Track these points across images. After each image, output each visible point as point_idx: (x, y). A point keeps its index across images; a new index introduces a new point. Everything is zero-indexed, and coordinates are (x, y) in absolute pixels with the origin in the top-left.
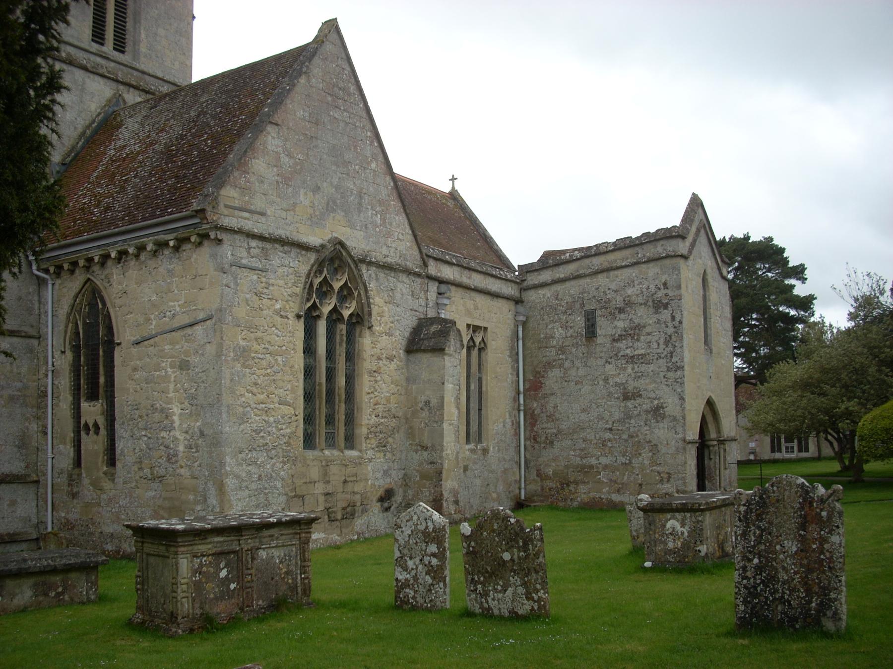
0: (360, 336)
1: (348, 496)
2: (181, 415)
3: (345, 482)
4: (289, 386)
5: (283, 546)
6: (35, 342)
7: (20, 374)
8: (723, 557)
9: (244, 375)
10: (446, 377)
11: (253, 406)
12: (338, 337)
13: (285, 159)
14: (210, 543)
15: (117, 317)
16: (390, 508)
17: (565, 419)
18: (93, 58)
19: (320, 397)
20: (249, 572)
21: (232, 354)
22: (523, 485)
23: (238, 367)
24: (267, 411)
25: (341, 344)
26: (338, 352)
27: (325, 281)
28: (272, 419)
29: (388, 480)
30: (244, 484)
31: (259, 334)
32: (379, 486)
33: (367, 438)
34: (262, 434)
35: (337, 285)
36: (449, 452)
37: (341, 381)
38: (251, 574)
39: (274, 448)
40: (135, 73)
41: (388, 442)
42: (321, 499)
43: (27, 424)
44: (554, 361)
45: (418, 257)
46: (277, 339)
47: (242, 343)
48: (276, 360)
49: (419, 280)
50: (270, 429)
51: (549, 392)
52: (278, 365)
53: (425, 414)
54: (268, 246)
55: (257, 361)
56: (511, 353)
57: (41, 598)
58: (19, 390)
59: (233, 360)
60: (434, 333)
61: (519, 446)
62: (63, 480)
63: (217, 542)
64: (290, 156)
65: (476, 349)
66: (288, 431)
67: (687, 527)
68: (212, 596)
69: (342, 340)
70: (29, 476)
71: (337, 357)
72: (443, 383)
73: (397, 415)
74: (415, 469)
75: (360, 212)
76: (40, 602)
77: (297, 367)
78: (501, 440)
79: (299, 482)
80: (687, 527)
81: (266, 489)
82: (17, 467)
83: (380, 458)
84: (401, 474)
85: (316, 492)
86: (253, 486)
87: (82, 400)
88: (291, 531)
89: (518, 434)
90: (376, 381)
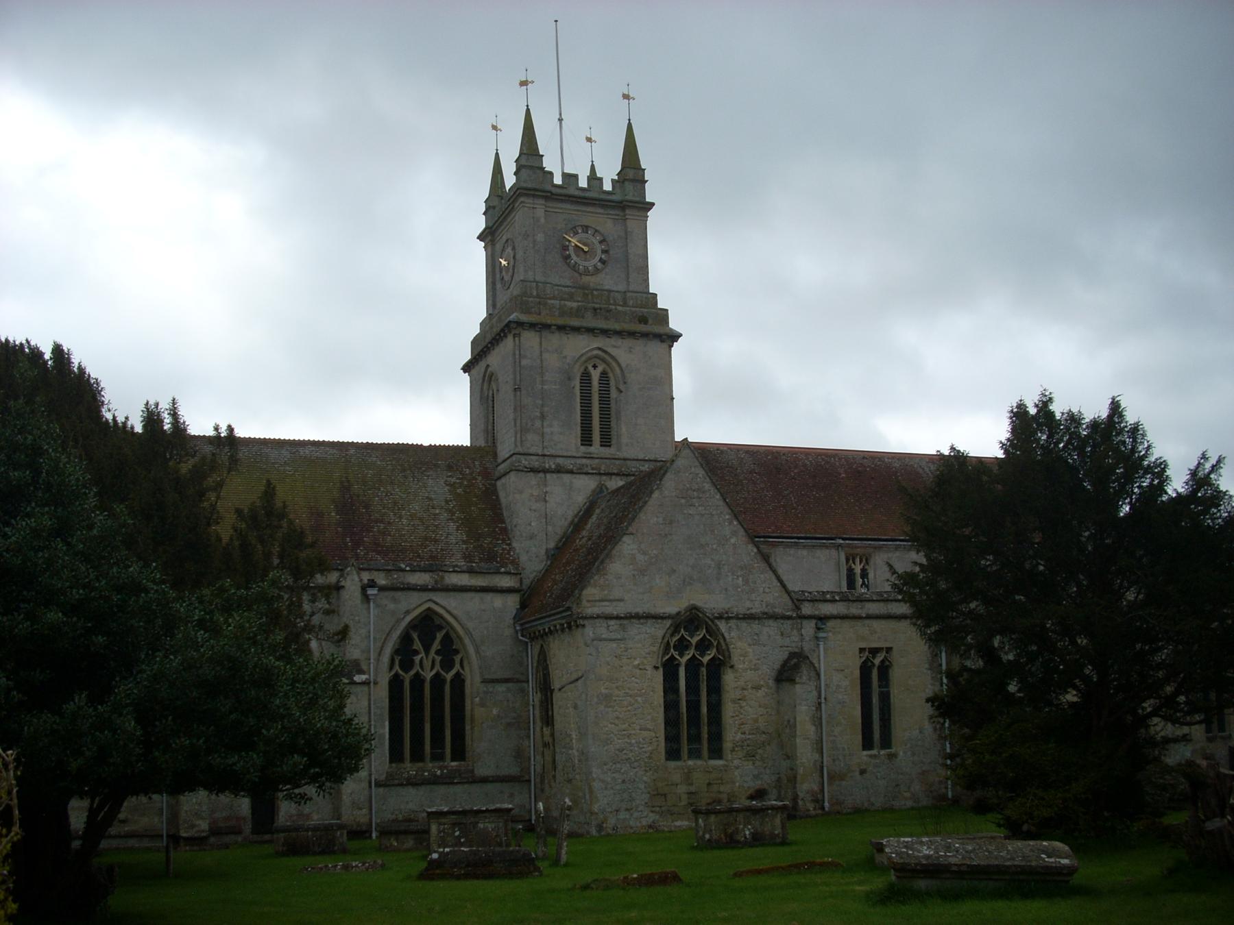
3: (709, 784)
13: (640, 557)
18: (579, 461)
23: (602, 707)
24: (629, 736)
27: (682, 638)
31: (620, 683)
35: (694, 641)
37: (704, 710)
40: (617, 462)
45: (790, 603)
47: (603, 691)
49: (789, 622)
53: (787, 731)
54: (625, 622)
64: (644, 553)
75: (718, 579)
82: (514, 770)
83: (748, 766)
84: (774, 778)
86: (618, 787)
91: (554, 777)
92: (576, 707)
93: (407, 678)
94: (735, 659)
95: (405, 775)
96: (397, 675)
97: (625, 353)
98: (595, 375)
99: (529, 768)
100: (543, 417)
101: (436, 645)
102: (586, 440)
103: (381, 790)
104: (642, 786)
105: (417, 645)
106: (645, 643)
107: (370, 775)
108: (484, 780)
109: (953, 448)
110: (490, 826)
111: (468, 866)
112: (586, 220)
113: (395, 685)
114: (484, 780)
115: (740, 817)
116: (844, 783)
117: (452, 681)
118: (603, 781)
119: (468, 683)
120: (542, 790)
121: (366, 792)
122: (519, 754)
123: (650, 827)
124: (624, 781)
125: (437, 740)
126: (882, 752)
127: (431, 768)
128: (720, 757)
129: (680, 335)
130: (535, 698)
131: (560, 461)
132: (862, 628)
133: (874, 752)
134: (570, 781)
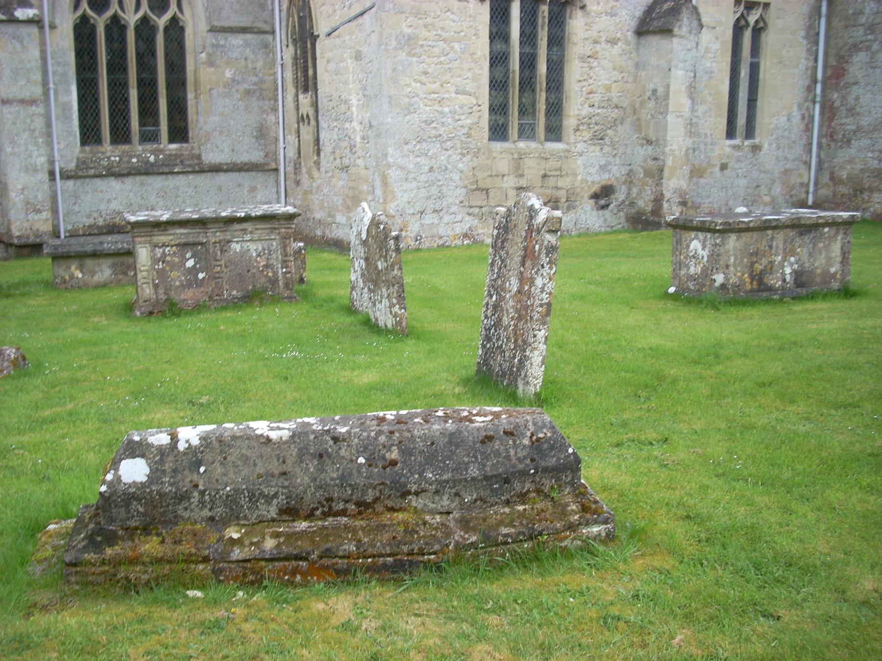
0: (570, 18)
1: (549, 191)
2: (357, 105)
3: (545, 176)
4: (469, 74)
5: (260, 240)
6: (269, 38)
7: (255, 68)
8: (759, 291)
9: (410, 64)
10: (674, 63)
11: (422, 95)
12: (540, 20)
14: (173, 234)
15: (315, 10)
16: (608, 206)
17: (867, 114)
19: (514, 86)
20: (218, 263)
21: (394, 43)
22: (811, 189)
23: (403, 56)
25: (543, 28)
26: (540, 37)
28: (446, 110)
29: (607, 176)
30: (411, 176)
31: (429, 20)
32: (593, 182)
33: (577, 130)
34: (434, 125)
36: (675, 147)
37: (542, 68)
38: (220, 266)
39: (450, 139)
41: (606, 135)
42: (512, 193)
43: (265, 116)
44: (861, 42)
46: (453, 24)
47: (407, 31)
48: (453, 47)
50: (444, 120)
51: (852, 80)
52: (455, 52)
53: (651, 104)
55: (427, 49)
56: (808, 33)
57: (120, 277)
58: (255, 84)
59: (396, 49)
60: (665, 12)
61: (811, 144)
62: (290, 169)
63: (181, 234)
65: (750, 29)
66: (469, 121)
67: (707, 250)
68: (178, 283)
69: (544, 23)
70: (268, 164)
71: (539, 42)
72: (670, 70)
73: (620, 105)
74: (639, 165)
76: (120, 280)
77: (479, 53)
78: (783, 137)
79: (481, 175)
80: (707, 250)
81: (439, 181)
82: (256, 156)
84: (624, 170)
85: (505, 185)
86: (423, 178)
87: (300, 92)
88: (268, 226)
89: (808, 129)
90: (591, 68)
91: (317, 164)
92: (358, 57)
93: (101, 22)
95: (105, 163)
96: (84, 18)
99: (275, 153)
103: (70, 183)
104: (456, 177)
107: (52, 162)
108: (216, 169)
110: (254, 248)
111: (290, 512)
113: (83, 33)
114: (216, 169)
115: (780, 238)
116: (702, 181)
117: (167, 29)
118: (402, 168)
119: (189, 32)
120: (298, 183)
121: (46, 187)
122: (262, 134)
123: (466, 236)
124: (431, 169)
125: (148, 112)
126: (747, 143)
127: (140, 152)
128: (559, 139)
130: (285, 53)
133: (737, 141)
134: (345, 168)
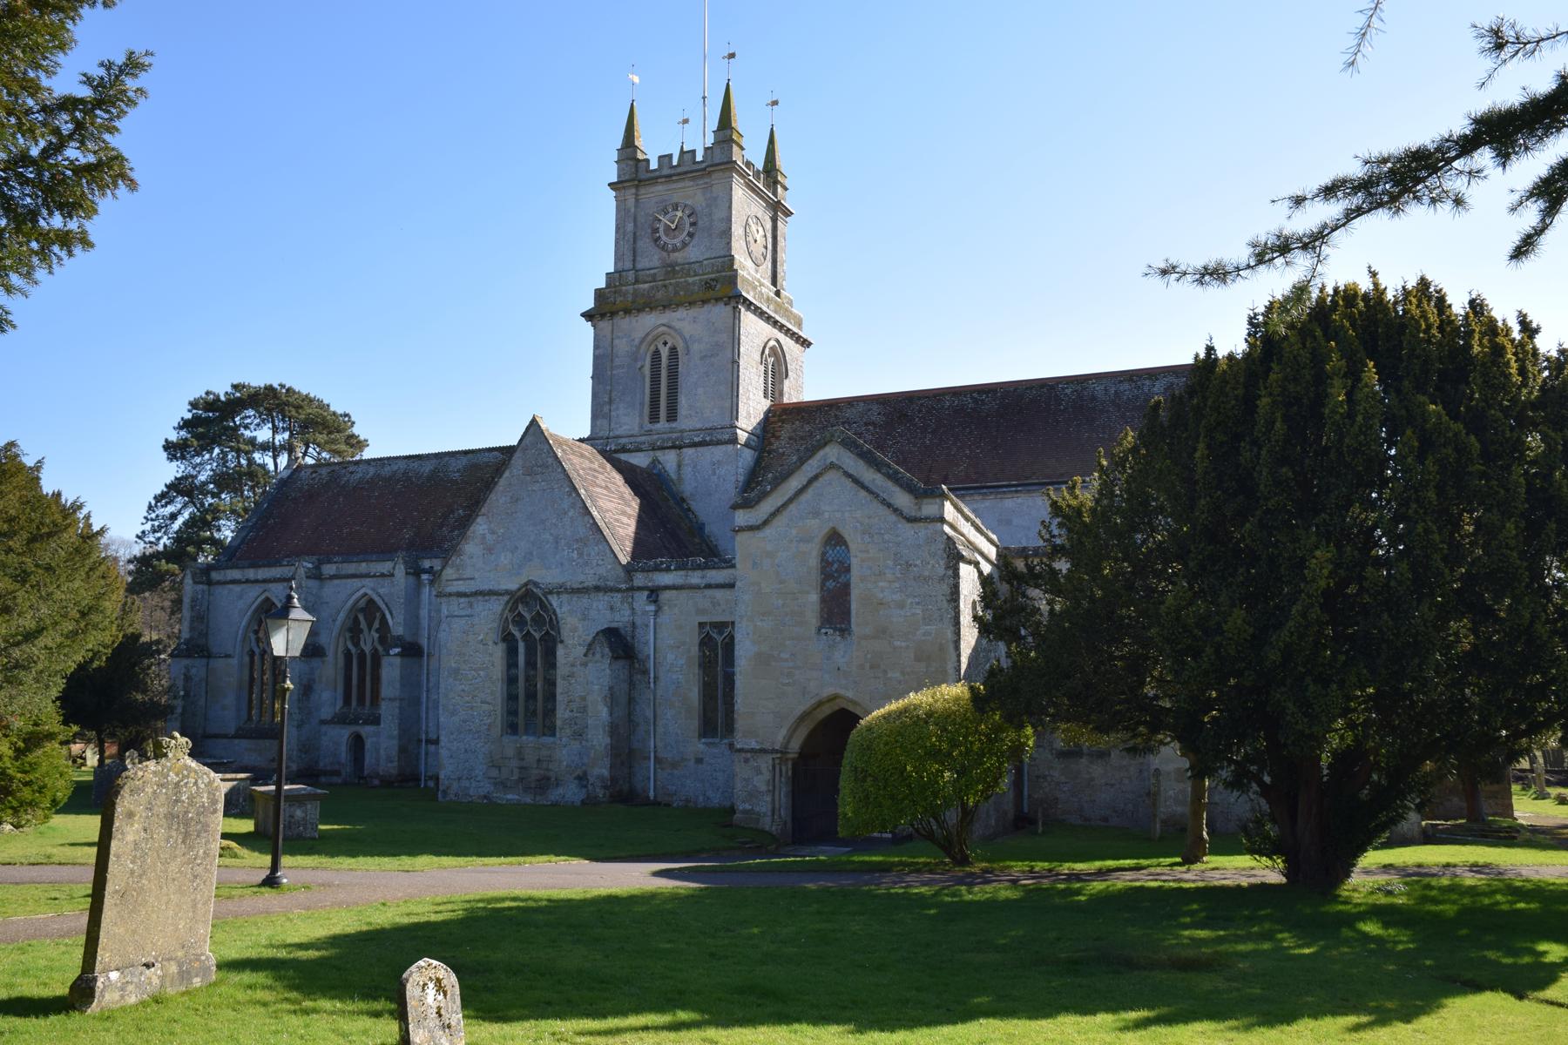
13: (489, 536)
64: (493, 533)
94: (565, 633)
97: (688, 324)
98: (665, 352)
100: (610, 402)
101: (376, 625)
102: (654, 418)
105: (363, 625)
106: (489, 615)
109: (39, 466)
112: (676, 198)
113: (348, 655)
128: (554, 735)
129: (583, 315)
131: (623, 441)
132: (702, 599)
